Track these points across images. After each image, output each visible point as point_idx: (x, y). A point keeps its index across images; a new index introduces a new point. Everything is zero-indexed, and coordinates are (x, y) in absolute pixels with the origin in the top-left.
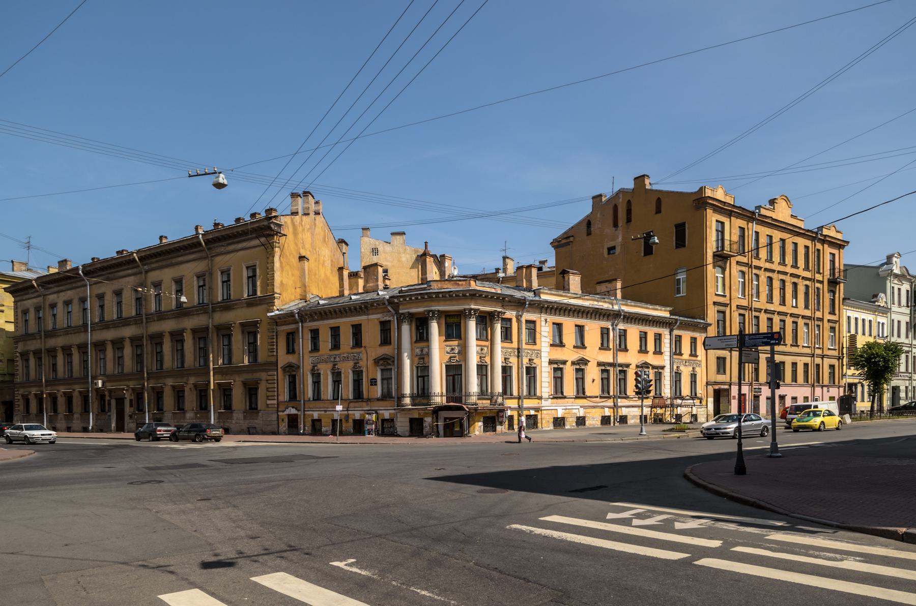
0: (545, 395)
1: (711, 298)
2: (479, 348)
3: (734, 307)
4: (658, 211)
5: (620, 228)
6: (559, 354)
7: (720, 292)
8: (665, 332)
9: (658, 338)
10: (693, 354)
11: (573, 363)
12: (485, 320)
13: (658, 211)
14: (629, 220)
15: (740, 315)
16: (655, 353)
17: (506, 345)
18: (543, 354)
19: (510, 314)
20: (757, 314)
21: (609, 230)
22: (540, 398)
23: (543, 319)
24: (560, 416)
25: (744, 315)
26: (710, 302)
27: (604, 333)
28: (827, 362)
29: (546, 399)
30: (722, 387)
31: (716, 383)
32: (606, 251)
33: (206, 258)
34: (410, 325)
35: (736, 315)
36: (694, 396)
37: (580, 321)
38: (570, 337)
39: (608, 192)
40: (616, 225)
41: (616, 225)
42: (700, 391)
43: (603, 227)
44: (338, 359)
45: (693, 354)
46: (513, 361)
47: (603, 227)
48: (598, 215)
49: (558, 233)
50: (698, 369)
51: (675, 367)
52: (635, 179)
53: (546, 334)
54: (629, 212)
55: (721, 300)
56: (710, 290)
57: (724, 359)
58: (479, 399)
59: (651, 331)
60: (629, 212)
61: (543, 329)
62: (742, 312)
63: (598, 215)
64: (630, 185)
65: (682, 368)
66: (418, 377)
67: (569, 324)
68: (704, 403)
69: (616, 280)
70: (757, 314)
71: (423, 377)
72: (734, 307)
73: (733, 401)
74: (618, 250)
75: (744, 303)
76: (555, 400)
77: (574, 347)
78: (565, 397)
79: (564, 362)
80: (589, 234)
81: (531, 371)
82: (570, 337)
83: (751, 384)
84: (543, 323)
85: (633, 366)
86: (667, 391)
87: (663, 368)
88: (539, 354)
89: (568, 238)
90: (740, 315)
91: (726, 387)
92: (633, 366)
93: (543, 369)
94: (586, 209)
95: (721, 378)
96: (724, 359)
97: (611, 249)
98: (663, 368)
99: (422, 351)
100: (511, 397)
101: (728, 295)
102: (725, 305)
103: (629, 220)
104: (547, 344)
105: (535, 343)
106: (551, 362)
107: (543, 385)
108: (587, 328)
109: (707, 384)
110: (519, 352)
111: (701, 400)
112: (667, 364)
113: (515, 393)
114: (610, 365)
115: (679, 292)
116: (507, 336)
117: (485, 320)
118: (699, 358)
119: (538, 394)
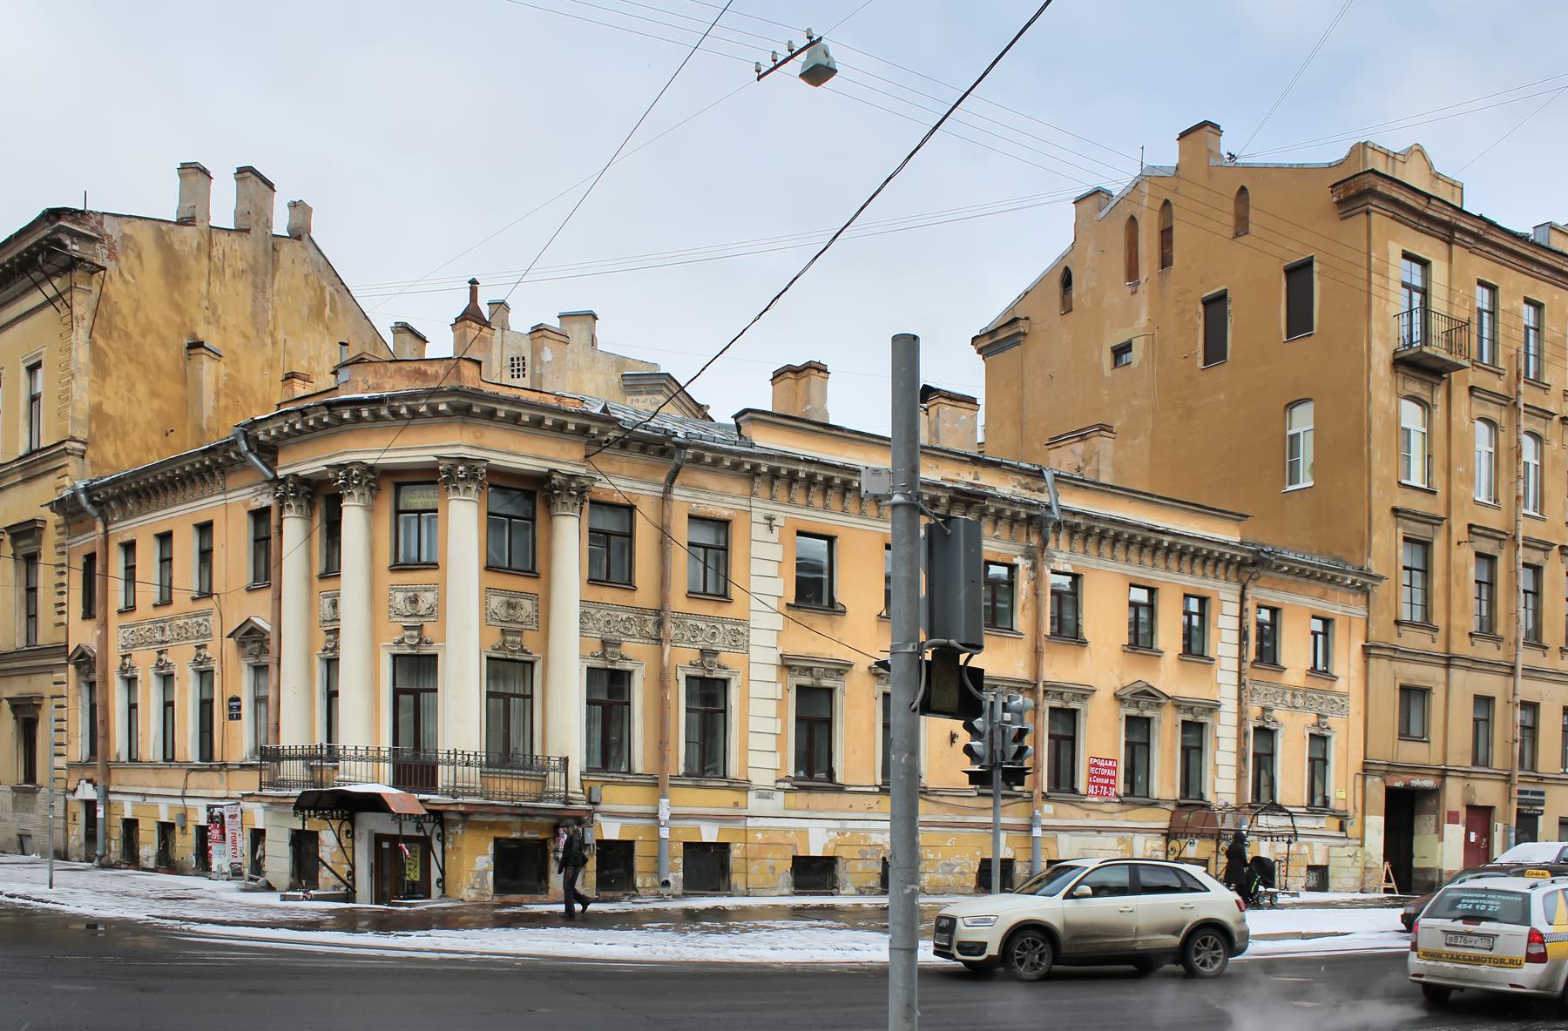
0: (762, 778)
1: (1383, 498)
2: (495, 602)
3: (1459, 531)
5: (1143, 287)
6: (817, 641)
7: (1417, 479)
8: (1225, 595)
10: (1321, 671)
12: (521, 503)
13: (1242, 226)
14: (1166, 261)
15: (1479, 555)
17: (608, 595)
18: (755, 638)
19: (621, 480)
20: (1536, 557)
21: (1116, 290)
22: (743, 787)
23: (758, 516)
24: (816, 850)
25: (1491, 559)
26: (1382, 515)
28: (1466, 684)
29: (765, 794)
30: (1417, 782)
31: (1391, 768)
32: (1107, 358)
34: (309, 518)
35: (1465, 557)
36: (1318, 804)
39: (1118, 181)
40: (1132, 273)
41: (1132, 273)
42: (1340, 790)
43: (1101, 282)
44: (168, 635)
45: (1321, 671)
46: (636, 655)
47: (1101, 282)
48: (1090, 253)
49: (989, 314)
50: (1334, 721)
52: (1183, 135)
53: (772, 569)
54: (1166, 236)
55: (1420, 504)
56: (1381, 468)
57: (1424, 692)
59: (1174, 583)
60: (1166, 236)
61: (757, 550)
62: (1487, 547)
63: (1090, 253)
64: (1168, 156)
65: (1279, 714)
66: (397, 693)
68: (1353, 829)
70: (1536, 557)
71: (416, 693)
72: (1459, 531)
73: (1448, 828)
74: (1136, 356)
75: (1494, 520)
76: (801, 796)
78: (840, 789)
79: (842, 669)
80: (1067, 307)
81: (709, 697)
83: (1508, 779)
84: (759, 531)
85: (1104, 696)
86: (1223, 782)
87: (1213, 708)
88: (739, 635)
89: (1015, 320)
90: (1479, 555)
91: (1428, 783)
92: (1104, 696)
93: (755, 689)
94: (1050, 237)
95: (1412, 753)
96: (1424, 692)
97: (1121, 351)
98: (1213, 708)
99: (414, 601)
101: (1441, 491)
102: (1432, 520)
103: (1166, 261)
105: (724, 597)
106: (787, 665)
107: (754, 741)
109: (1367, 769)
110: (660, 624)
111: (1343, 820)
112: (1227, 695)
115: (1294, 479)
118: (1340, 686)
119: (734, 770)
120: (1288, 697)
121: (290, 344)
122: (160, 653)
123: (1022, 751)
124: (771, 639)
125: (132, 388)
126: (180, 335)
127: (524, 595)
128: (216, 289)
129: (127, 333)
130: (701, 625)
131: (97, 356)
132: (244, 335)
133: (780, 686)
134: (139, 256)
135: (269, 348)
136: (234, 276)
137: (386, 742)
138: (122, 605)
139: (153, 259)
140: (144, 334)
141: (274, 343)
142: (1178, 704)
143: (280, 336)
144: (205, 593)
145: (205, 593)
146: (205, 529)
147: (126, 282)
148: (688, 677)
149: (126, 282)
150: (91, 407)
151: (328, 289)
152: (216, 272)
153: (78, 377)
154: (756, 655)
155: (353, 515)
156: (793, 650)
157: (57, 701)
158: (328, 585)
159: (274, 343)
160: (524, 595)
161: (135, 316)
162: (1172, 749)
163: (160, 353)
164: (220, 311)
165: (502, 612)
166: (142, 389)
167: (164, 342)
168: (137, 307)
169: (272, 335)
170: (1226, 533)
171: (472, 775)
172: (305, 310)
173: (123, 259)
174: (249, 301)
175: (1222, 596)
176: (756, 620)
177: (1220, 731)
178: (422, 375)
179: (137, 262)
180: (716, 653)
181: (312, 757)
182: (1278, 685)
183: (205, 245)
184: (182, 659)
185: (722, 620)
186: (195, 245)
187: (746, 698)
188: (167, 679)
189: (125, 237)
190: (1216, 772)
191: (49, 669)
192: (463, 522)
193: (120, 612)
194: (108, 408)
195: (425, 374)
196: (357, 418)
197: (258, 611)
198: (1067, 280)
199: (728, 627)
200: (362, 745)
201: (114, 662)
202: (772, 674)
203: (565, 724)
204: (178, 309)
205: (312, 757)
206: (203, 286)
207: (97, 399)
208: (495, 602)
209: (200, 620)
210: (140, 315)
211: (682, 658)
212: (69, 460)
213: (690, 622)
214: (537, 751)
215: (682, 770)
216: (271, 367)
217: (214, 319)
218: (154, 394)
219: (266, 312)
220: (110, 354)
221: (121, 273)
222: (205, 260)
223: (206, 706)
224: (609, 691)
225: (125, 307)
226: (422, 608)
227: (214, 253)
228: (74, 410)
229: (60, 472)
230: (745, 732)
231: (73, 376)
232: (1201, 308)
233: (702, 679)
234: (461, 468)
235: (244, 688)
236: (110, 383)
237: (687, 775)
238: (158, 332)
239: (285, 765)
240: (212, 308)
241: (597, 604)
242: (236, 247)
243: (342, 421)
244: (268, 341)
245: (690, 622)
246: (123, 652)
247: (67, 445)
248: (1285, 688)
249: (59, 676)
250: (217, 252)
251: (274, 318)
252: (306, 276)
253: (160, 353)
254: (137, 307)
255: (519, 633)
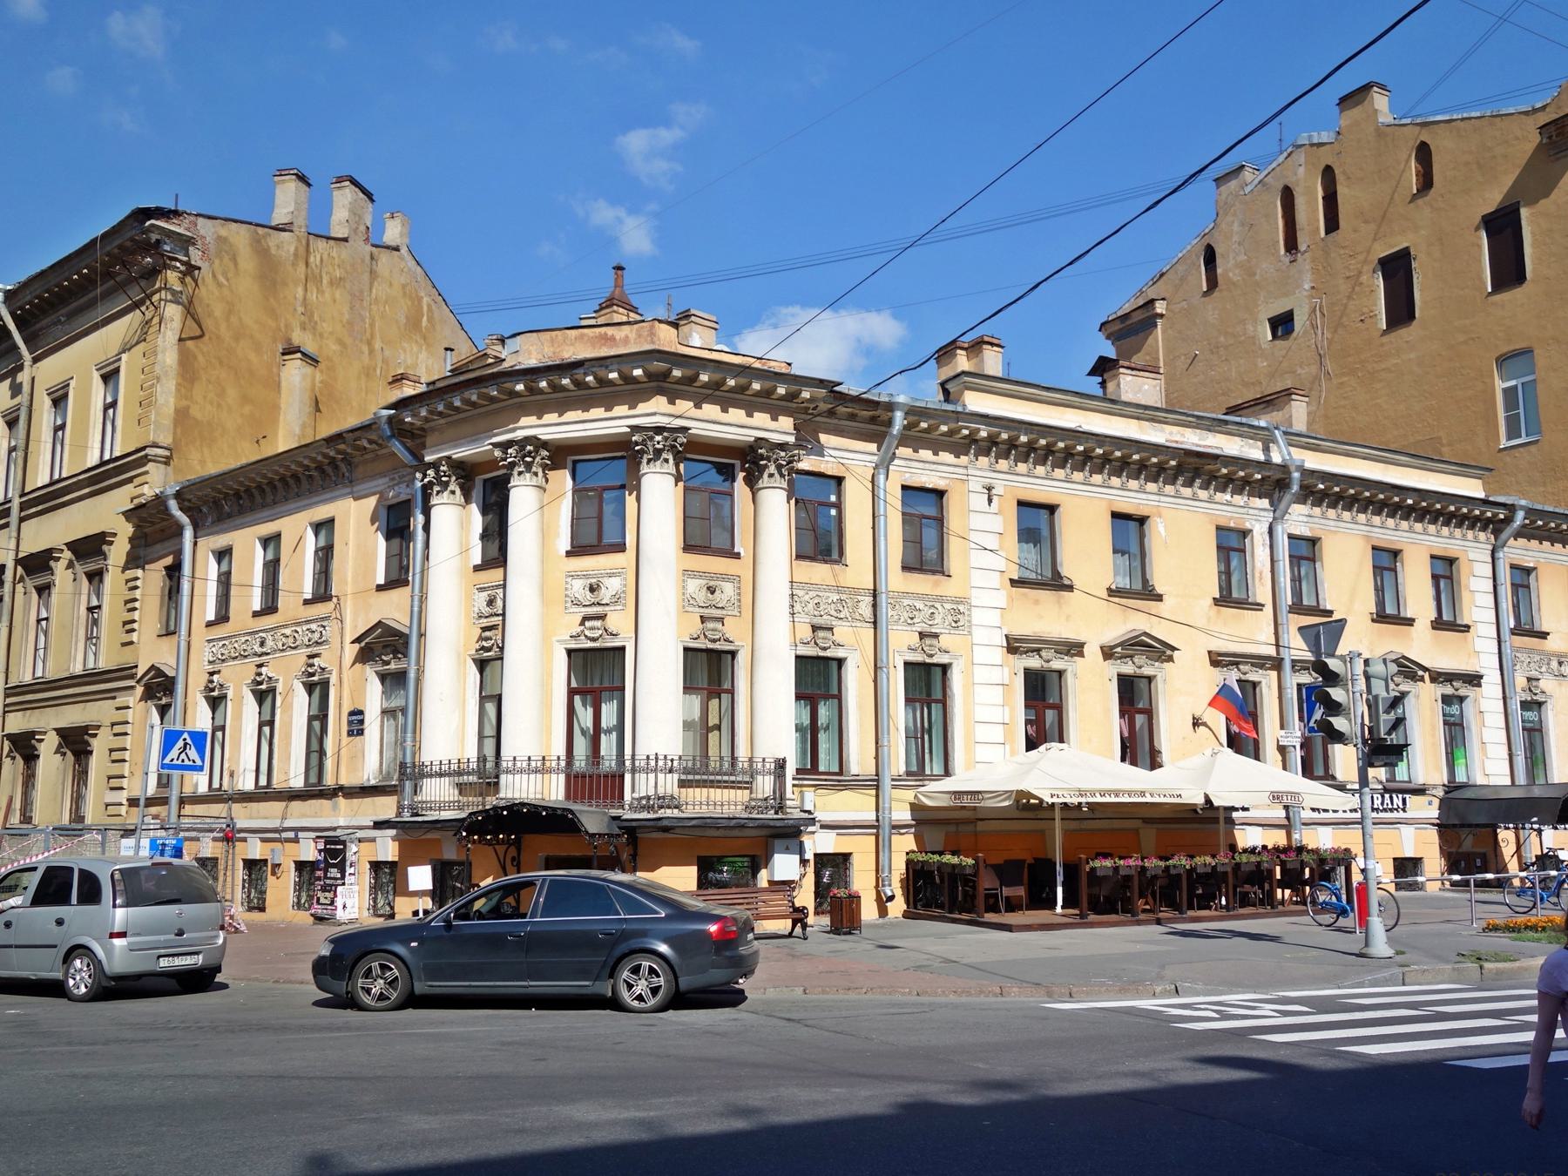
2: (694, 586)
4: (1401, 310)
6: (1045, 617)
9: (1445, 571)
11: (1108, 653)
12: (721, 468)
13: (1401, 310)
16: (1439, 624)
17: (819, 572)
18: (978, 616)
23: (976, 485)
24: (1409, 854)
27: (1231, 544)
33: (136, 305)
37: (1134, 496)
38: (1086, 549)
41: (1291, 244)
46: (852, 644)
51: (1521, 681)
54: (1331, 200)
58: (683, 784)
59: (1419, 544)
60: (1331, 200)
65: (1547, 684)
67: (1084, 505)
69: (1287, 394)
74: (1300, 321)
77: (1112, 592)
79: (1074, 649)
81: (928, 683)
82: (1086, 549)
84: (979, 501)
88: (959, 615)
93: (980, 674)
97: (1282, 324)
98: (1474, 680)
100: (840, 779)
103: (1332, 224)
104: (995, 580)
108: (1158, 531)
112: (1487, 665)
113: (859, 760)
114: (1260, 662)
116: (820, 541)
117: (721, 468)
120: (1554, 664)
121: (387, 353)
122: (212, 674)
123: (1399, 722)
124: (994, 618)
125: (222, 393)
126: (275, 341)
127: (725, 577)
128: (313, 296)
129: (218, 337)
130: (919, 605)
131: (185, 361)
132: (340, 342)
133: (1006, 670)
134: (234, 259)
135: (366, 358)
136: (331, 283)
137: (559, 749)
138: (211, 616)
139: (248, 262)
140: (237, 338)
141: (371, 352)
142: (1438, 677)
143: (378, 345)
144: (322, 594)
145: (322, 594)
146: (324, 527)
147: (220, 285)
148: (907, 664)
149: (220, 285)
150: (177, 411)
151: (426, 300)
152: (311, 279)
153: (164, 380)
154: (979, 635)
155: (523, 496)
156: (1018, 631)
157: (118, 729)
158: (495, 575)
159: (371, 352)
160: (725, 577)
161: (227, 319)
162: (1433, 728)
163: (253, 357)
164: (316, 318)
165: (702, 596)
166: (232, 394)
167: (258, 347)
168: (230, 311)
169: (369, 343)
170: (1471, 488)
171: (668, 784)
172: (403, 320)
173: (217, 262)
174: (346, 309)
175: (1471, 556)
176: (977, 598)
177: (1485, 705)
178: (611, 340)
179: (231, 265)
180: (936, 636)
181: (459, 773)
182: (1541, 652)
183: (302, 250)
184: (286, 674)
185: (941, 599)
186: (292, 249)
187: (970, 684)
188: (264, 694)
189: (221, 240)
190: (1484, 751)
191: (110, 694)
192: (659, 497)
193: (209, 624)
194: (195, 412)
195: (613, 339)
196: (532, 390)
197: (394, 609)
198: (1210, 257)
199: (948, 606)
200: (536, 754)
201: (197, 681)
202: (998, 655)
203: (770, 719)
204: (273, 313)
205: (459, 773)
206: (300, 291)
207: (184, 403)
208: (694, 586)
209: (314, 626)
210: (233, 319)
211: (902, 645)
212: (150, 467)
213: (906, 602)
214: (742, 752)
215: (902, 769)
216: (368, 375)
217: (309, 324)
218: (245, 399)
219: (363, 320)
220: (200, 358)
221: (214, 276)
222: (302, 268)
223: (319, 718)
224: (817, 679)
225: (218, 309)
226: (605, 595)
227: (312, 259)
228: (157, 414)
229: (137, 481)
230: (972, 723)
231: (158, 379)
232: (231, 615)
233: (924, 664)
234: (658, 438)
235: (373, 698)
236: (198, 391)
237: (908, 773)
238: (252, 337)
239: (427, 782)
240: (308, 312)
241: (809, 586)
242: (334, 254)
243: (513, 394)
244: (365, 349)
245: (906, 602)
246: (210, 668)
247: (148, 451)
248: (1549, 656)
249: (122, 700)
250: (314, 259)
251: (372, 325)
252: (404, 286)
253: (253, 357)
254: (230, 311)
255: (721, 620)
